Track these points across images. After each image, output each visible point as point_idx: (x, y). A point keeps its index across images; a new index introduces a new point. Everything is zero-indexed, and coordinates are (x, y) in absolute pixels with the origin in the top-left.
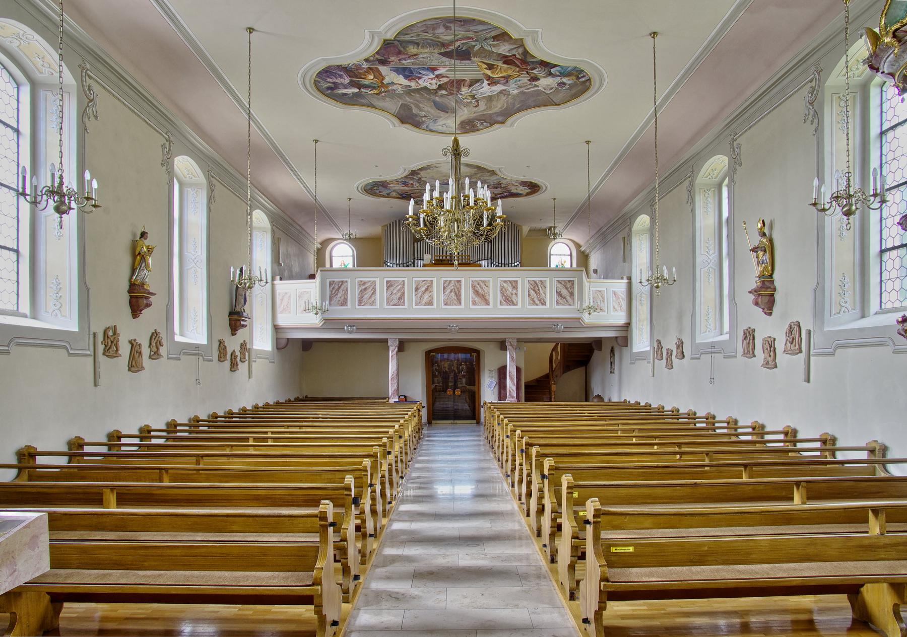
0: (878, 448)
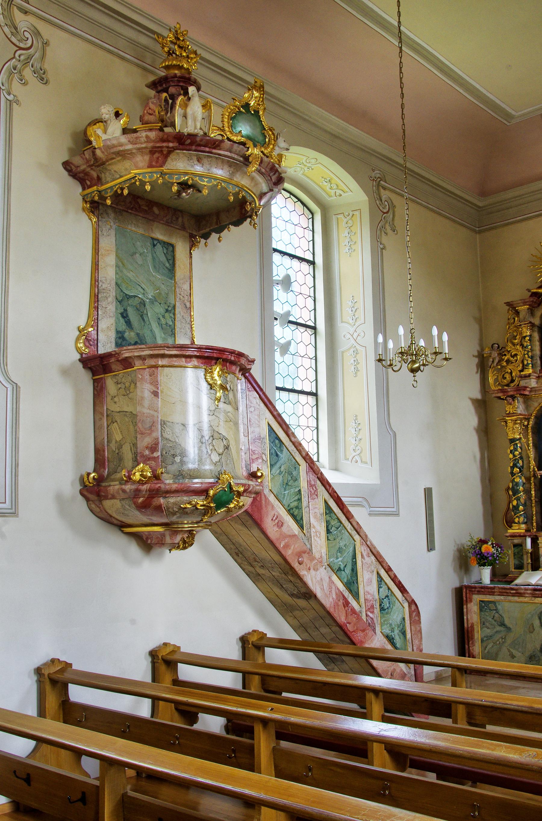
0: (157, 434)
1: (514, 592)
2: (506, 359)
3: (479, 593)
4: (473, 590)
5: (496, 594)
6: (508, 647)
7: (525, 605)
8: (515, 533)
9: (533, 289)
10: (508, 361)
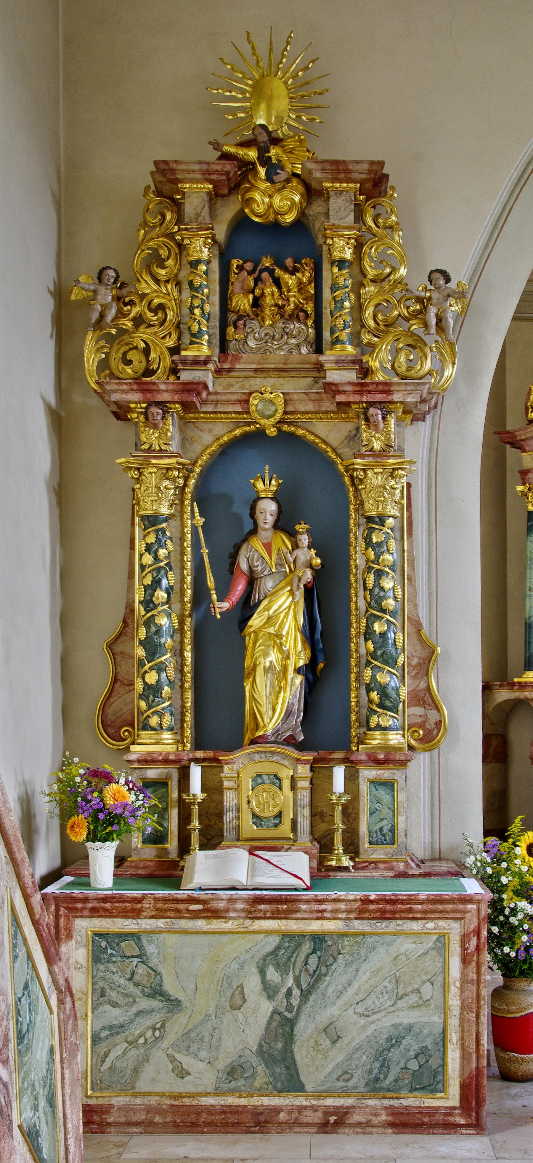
1: (200, 907)
2: (133, 314)
3: (95, 912)
4: (80, 905)
5: (145, 914)
6: (170, 1051)
7: (225, 939)
8: (153, 752)
9: (227, 145)
10: (139, 321)
